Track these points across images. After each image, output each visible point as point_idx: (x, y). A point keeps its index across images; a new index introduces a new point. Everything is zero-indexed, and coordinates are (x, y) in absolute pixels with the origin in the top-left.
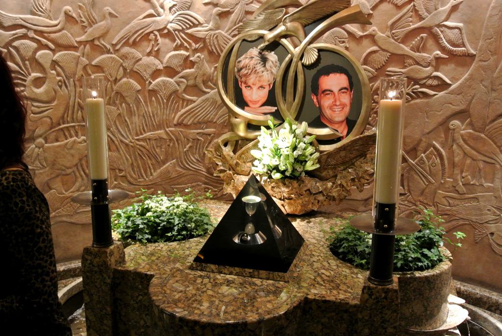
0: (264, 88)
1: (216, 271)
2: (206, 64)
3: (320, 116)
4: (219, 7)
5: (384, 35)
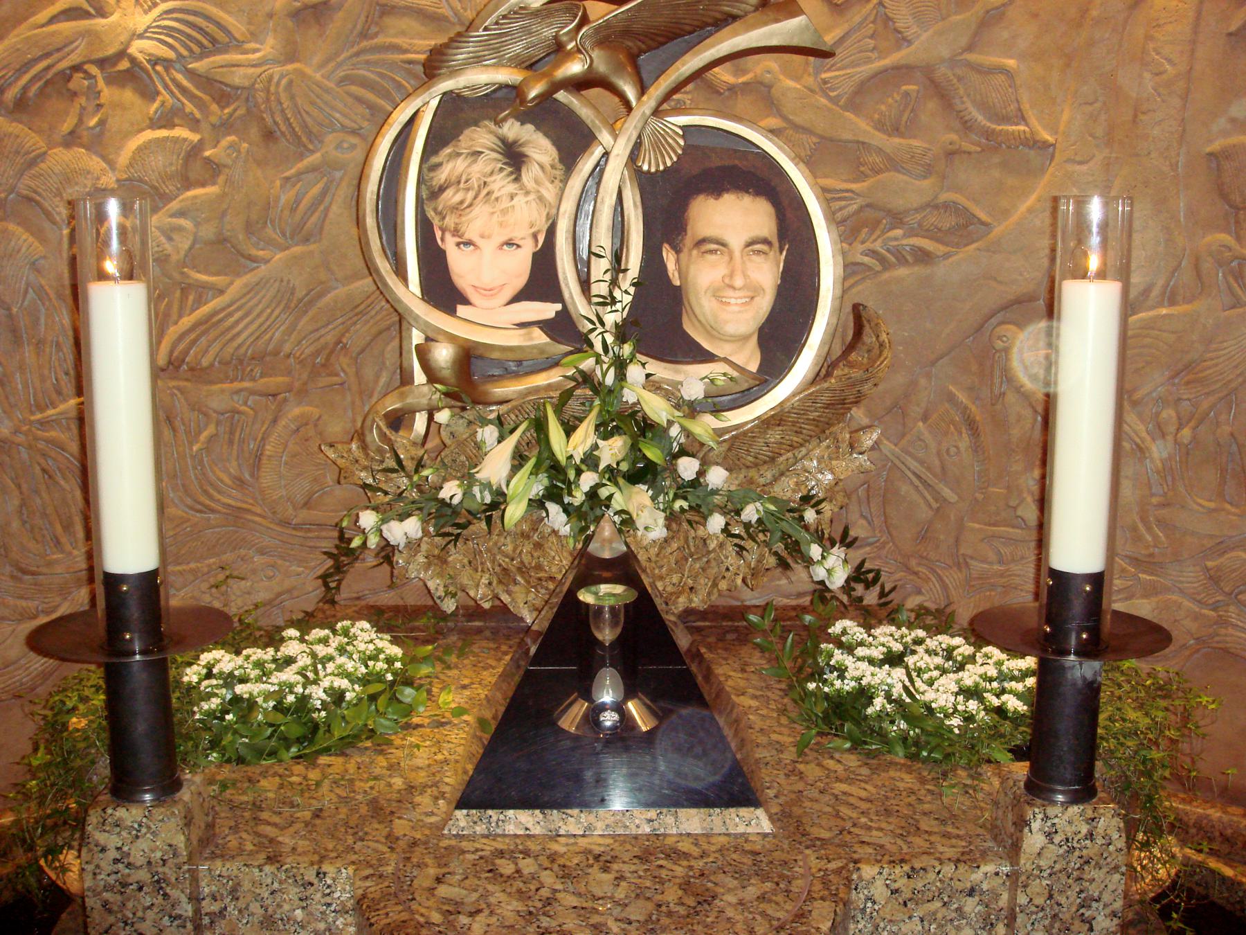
0: (518, 246)
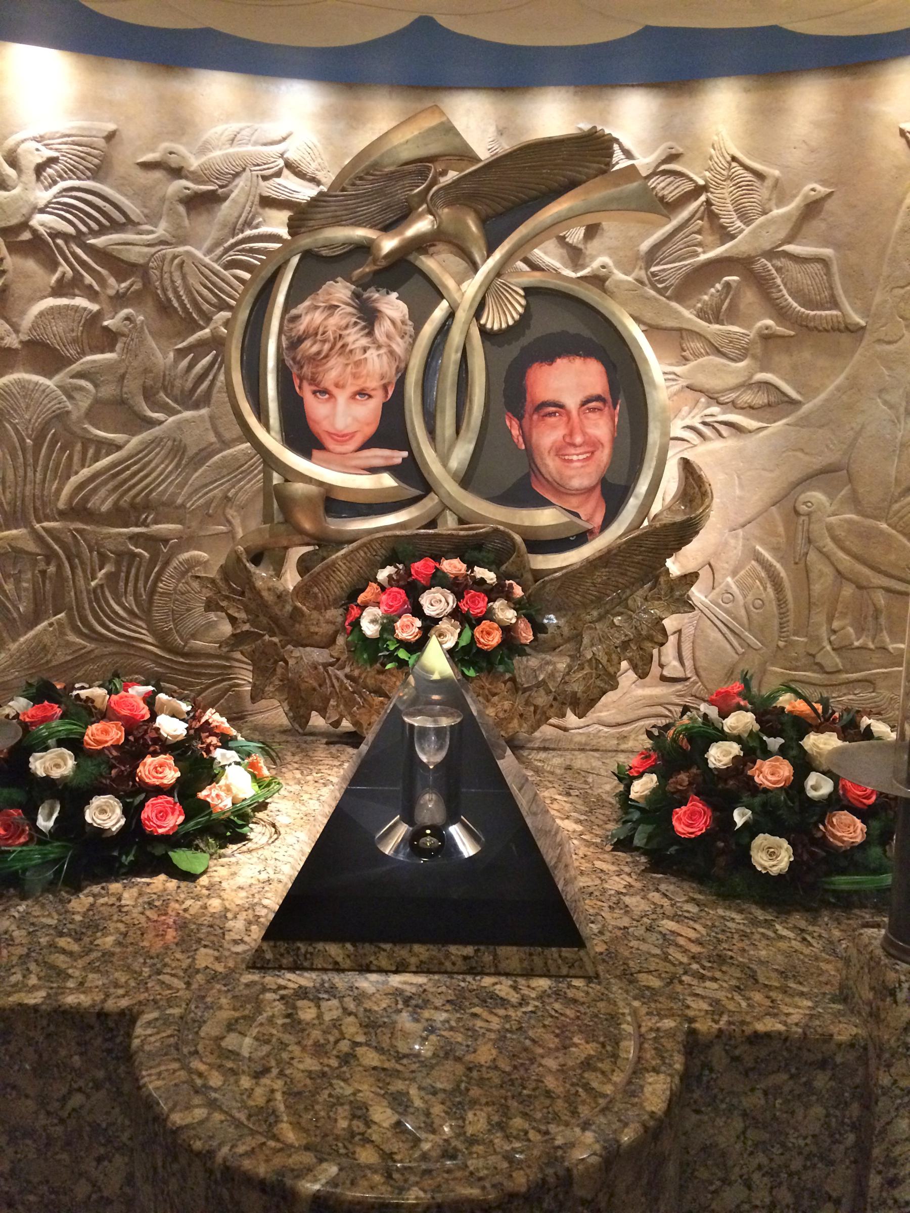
0: (370, 396)
1: (348, 963)
2: (151, 342)
3: (528, 476)
4: (186, 178)
5: (630, 279)
